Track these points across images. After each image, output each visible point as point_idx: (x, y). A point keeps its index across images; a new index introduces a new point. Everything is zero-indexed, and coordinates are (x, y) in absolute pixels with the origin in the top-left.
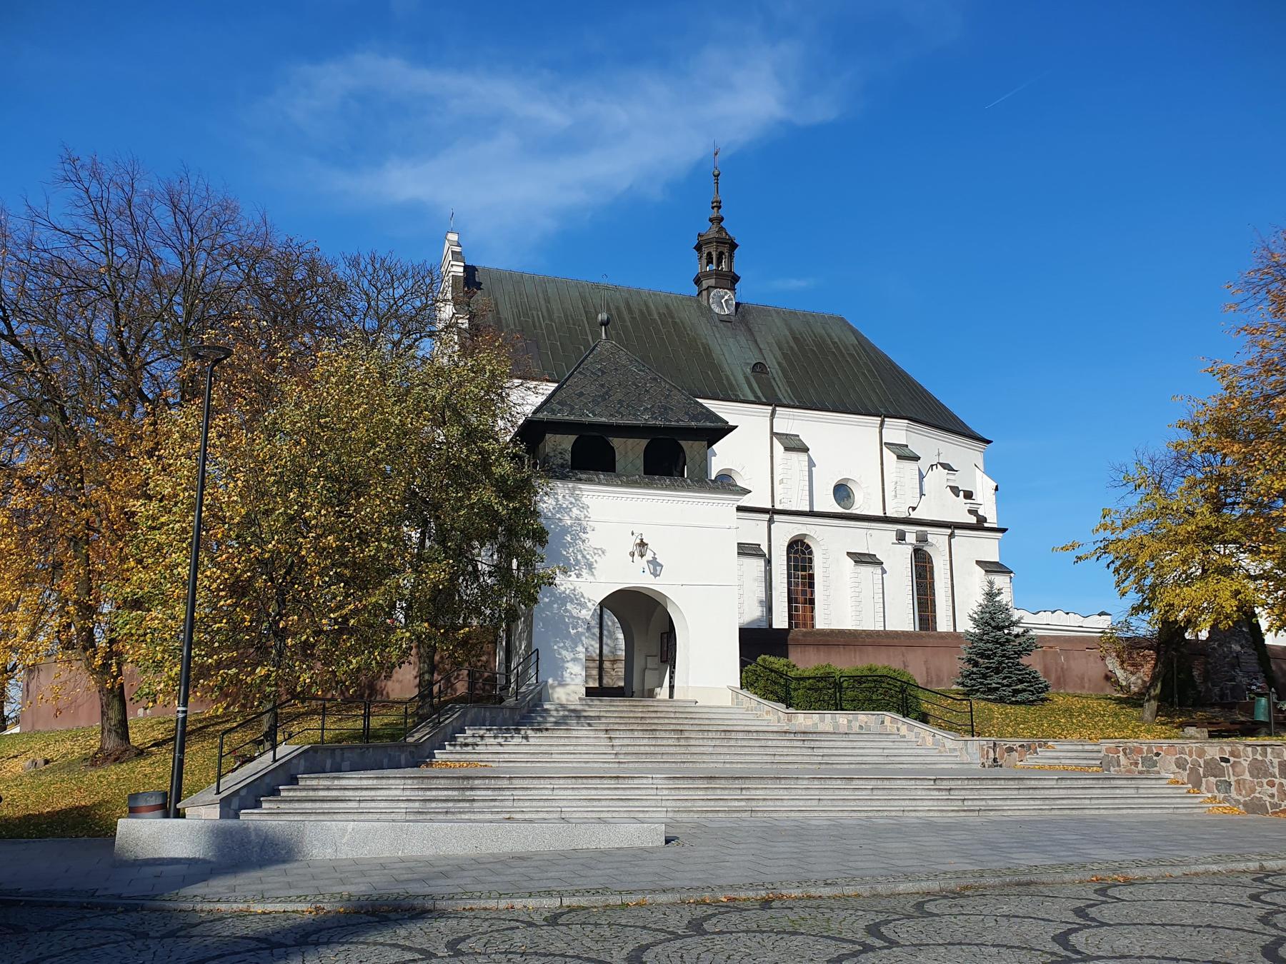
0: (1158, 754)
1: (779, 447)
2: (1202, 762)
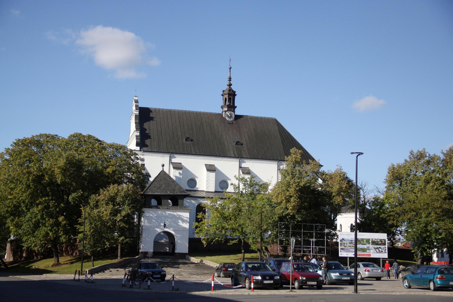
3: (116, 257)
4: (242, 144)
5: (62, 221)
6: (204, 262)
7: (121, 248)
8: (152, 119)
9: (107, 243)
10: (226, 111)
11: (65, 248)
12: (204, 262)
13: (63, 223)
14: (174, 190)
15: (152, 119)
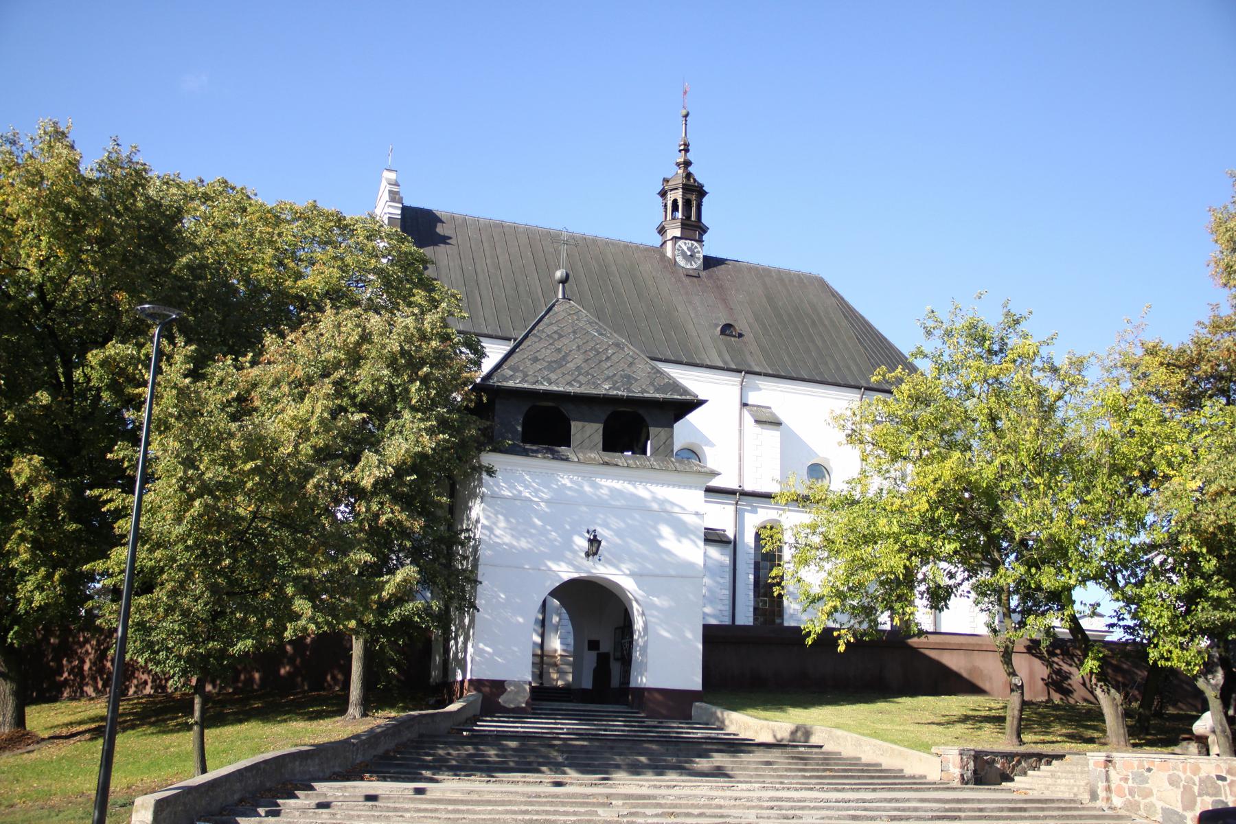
0: (1149, 770)
1: (748, 419)
2: (1196, 779)
3: (340, 708)
4: (741, 335)
5: (32, 482)
6: (814, 740)
7: (368, 655)
8: (444, 240)
9: (302, 605)
10: (675, 239)
11: (93, 663)
12: (814, 740)
13: (35, 492)
14: (629, 377)
15: (444, 240)
